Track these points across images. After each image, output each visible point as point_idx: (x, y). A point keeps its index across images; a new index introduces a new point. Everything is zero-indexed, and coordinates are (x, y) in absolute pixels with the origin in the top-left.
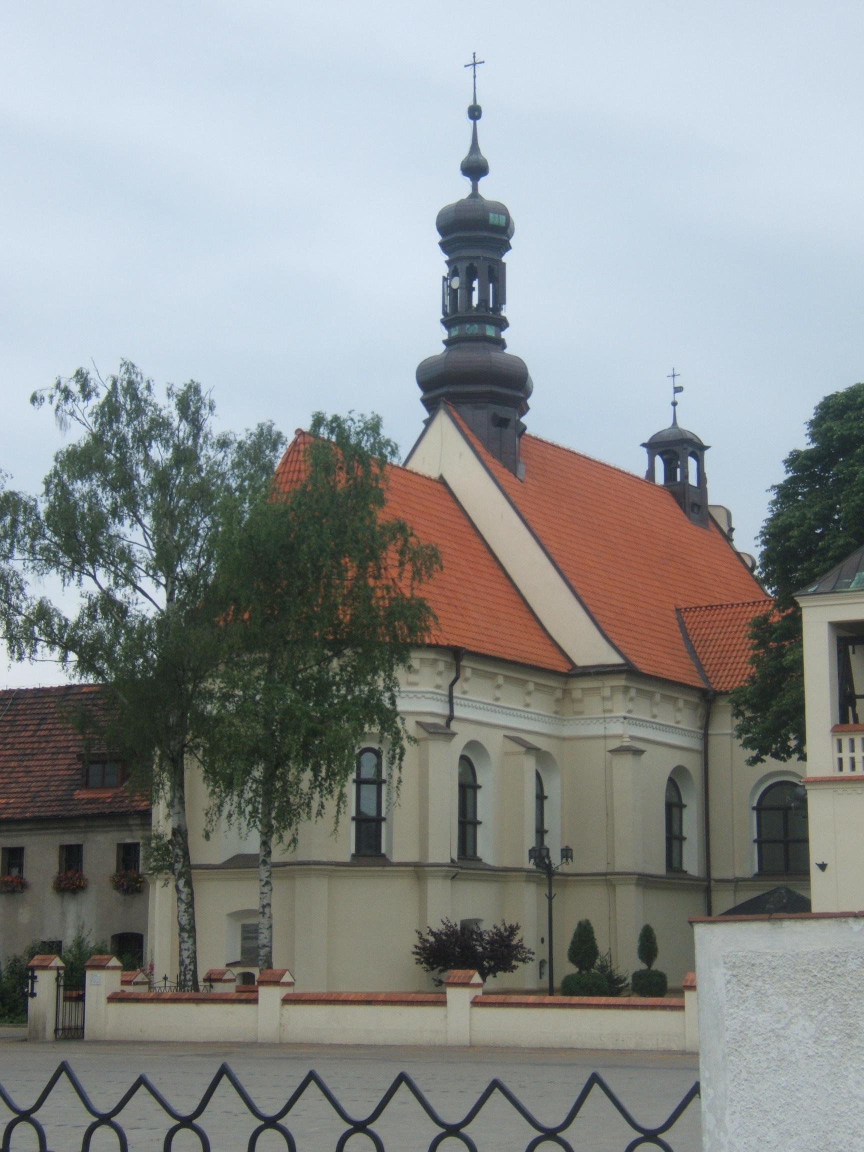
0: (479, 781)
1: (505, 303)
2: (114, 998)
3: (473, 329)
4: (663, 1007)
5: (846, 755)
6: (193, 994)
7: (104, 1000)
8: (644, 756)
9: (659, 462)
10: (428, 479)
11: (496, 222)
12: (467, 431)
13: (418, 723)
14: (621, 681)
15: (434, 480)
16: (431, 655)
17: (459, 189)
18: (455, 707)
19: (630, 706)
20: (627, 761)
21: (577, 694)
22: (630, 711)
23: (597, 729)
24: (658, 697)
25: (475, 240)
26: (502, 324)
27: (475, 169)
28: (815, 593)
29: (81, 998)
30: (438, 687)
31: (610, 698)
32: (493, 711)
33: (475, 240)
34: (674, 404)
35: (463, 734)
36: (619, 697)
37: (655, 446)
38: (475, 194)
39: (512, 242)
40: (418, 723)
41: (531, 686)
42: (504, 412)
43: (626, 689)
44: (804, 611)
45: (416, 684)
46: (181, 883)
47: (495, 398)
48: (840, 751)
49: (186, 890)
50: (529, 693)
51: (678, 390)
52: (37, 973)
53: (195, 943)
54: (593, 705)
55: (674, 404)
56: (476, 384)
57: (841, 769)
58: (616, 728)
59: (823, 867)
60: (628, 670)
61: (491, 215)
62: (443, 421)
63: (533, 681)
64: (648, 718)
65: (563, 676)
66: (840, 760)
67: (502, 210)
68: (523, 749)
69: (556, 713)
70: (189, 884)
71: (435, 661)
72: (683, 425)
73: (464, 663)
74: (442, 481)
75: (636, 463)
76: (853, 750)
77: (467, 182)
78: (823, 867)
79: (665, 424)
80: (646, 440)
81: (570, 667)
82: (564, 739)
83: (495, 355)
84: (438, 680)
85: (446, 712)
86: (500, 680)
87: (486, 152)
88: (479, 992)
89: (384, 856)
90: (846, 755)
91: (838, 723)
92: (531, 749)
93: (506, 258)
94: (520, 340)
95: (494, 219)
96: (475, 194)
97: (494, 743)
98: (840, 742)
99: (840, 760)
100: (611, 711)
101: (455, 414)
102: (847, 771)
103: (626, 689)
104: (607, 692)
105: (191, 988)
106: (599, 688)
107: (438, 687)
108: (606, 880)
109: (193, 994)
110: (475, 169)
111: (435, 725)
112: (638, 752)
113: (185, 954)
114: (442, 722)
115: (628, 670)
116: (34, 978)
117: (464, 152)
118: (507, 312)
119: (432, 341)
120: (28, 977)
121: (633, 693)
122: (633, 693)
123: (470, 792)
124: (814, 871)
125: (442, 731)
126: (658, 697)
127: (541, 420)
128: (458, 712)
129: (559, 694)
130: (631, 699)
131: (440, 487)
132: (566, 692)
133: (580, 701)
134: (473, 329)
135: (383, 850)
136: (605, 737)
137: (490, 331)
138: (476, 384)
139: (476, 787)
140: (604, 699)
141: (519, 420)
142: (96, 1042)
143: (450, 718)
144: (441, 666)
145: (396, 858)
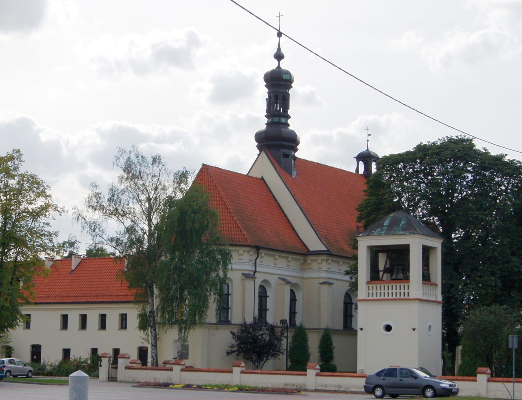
0: (268, 294)
1: (289, 109)
2: (127, 368)
3: (276, 119)
4: (301, 375)
5: (371, 292)
6: (156, 367)
7: (124, 368)
8: (333, 285)
9: (361, 164)
10: (257, 178)
11: (286, 78)
12: (272, 159)
13: (243, 274)
14: (325, 257)
15: (259, 179)
16: (247, 249)
17: (272, 65)
18: (257, 267)
19: (329, 266)
20: (326, 287)
21: (309, 261)
22: (328, 268)
23: (316, 275)
24: (341, 263)
25: (279, 85)
26: (288, 117)
27: (279, 56)
28: (362, 236)
29: (117, 368)
30: (251, 260)
31: (321, 263)
32: (273, 269)
33: (279, 85)
34: (368, 141)
35: (259, 279)
36: (324, 263)
37: (361, 157)
38: (279, 67)
39: (292, 85)
40: (243, 274)
41: (290, 259)
42: (287, 151)
43: (327, 260)
44: (359, 242)
45: (242, 259)
46: (152, 330)
47: (284, 147)
48: (369, 290)
49: (154, 332)
50: (289, 261)
51: (369, 135)
52: (102, 359)
53: (157, 350)
54: (315, 266)
55: (368, 141)
56: (276, 141)
57: (369, 296)
58: (323, 275)
59: (361, 329)
60: (327, 253)
61: (284, 75)
62: (263, 154)
63: (291, 257)
64: (337, 271)
65: (304, 253)
66: (408, 289)
67: (288, 73)
68: (284, 283)
69: (301, 268)
70: (155, 330)
71: (249, 251)
72: (370, 149)
73: (261, 251)
74: (262, 179)
75: (350, 166)
76: (381, 290)
77: (276, 61)
78: (361, 329)
79: (364, 149)
80: (356, 156)
81: (306, 251)
82: (304, 278)
83: (283, 129)
84: (251, 258)
85: (254, 269)
86: (277, 257)
87: (283, 51)
88: (244, 369)
89: (229, 321)
90: (371, 292)
91: (369, 280)
92: (288, 282)
93: (290, 92)
94: (294, 124)
95: (285, 77)
96: (279, 67)
97: (273, 280)
98: (369, 287)
99: (369, 293)
100: (321, 268)
101: (268, 153)
102: (371, 297)
103: (327, 260)
104: (320, 261)
105: (156, 366)
106: (317, 260)
107: (251, 260)
108: (318, 331)
109: (156, 367)
110: (279, 56)
111: (249, 274)
112: (331, 284)
113: (154, 354)
114: (252, 273)
115: (327, 253)
116: (101, 360)
117: (275, 51)
118: (290, 112)
119: (262, 124)
120: (99, 360)
121: (330, 261)
122: (330, 261)
123: (264, 299)
124: (359, 332)
125: (250, 276)
126: (341, 263)
127: (303, 153)
128: (258, 269)
129: (302, 261)
130: (329, 264)
131: (262, 182)
132: (305, 261)
133: (310, 264)
134: (276, 119)
135: (229, 319)
136: (319, 278)
137: (283, 120)
138: (276, 141)
139: (266, 297)
140: (319, 263)
141: (294, 155)
142: (121, 382)
143: (255, 272)
144: (252, 253)
145: (233, 322)
